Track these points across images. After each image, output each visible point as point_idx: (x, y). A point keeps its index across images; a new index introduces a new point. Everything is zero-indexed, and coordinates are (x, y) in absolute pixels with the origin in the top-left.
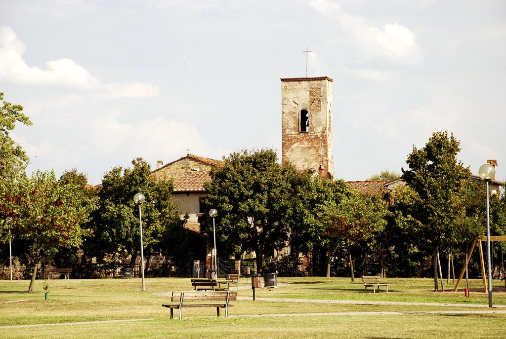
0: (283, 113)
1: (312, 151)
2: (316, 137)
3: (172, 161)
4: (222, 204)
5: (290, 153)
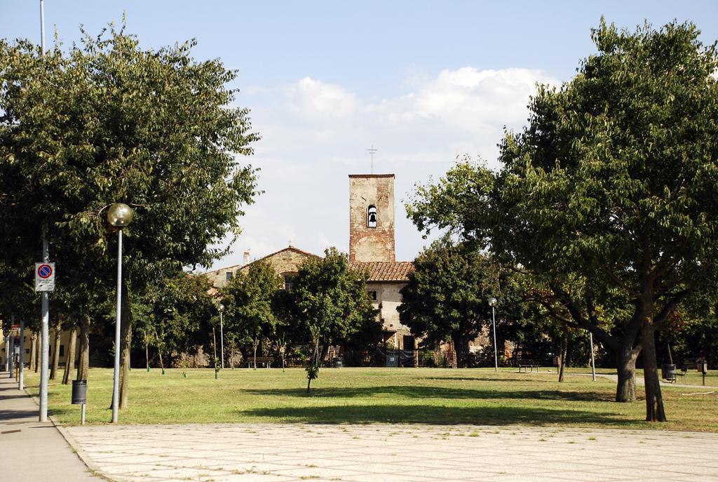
0: (351, 208)
1: (380, 246)
2: (384, 232)
4: (434, 294)
5: (358, 247)
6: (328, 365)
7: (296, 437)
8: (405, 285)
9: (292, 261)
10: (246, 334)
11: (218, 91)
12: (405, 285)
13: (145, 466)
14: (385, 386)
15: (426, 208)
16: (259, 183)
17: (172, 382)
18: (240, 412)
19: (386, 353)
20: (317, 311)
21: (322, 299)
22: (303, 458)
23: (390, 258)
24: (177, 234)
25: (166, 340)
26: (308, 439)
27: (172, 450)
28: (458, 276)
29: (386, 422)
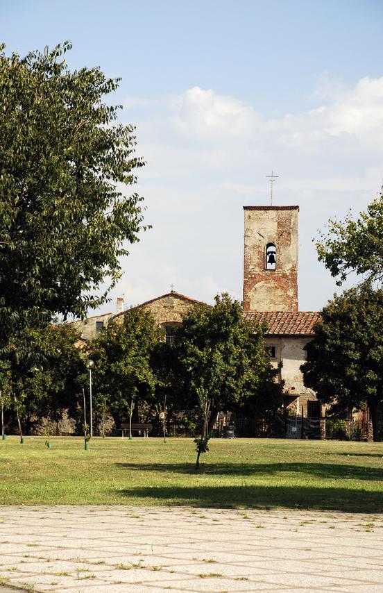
0: (246, 246)
1: (279, 292)
2: (285, 276)
3: (152, 299)
6: (217, 435)
7: (188, 524)
8: (313, 339)
9: (175, 310)
10: (118, 396)
11: (96, 106)
12: (311, 340)
13: (11, 558)
14: (289, 462)
15: (342, 248)
16: (147, 214)
17: (33, 453)
18: (118, 492)
19: (287, 422)
20: (204, 369)
21: (211, 355)
22: (199, 551)
23: (291, 307)
24: (47, 276)
25: (26, 402)
26: (202, 527)
27: (41, 538)
28: (376, 330)
29: (294, 507)
